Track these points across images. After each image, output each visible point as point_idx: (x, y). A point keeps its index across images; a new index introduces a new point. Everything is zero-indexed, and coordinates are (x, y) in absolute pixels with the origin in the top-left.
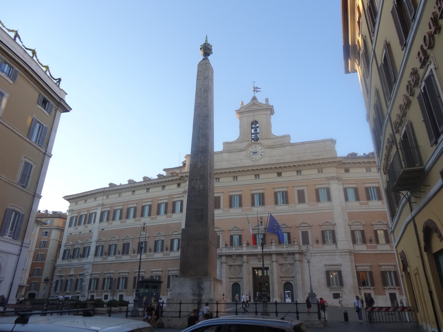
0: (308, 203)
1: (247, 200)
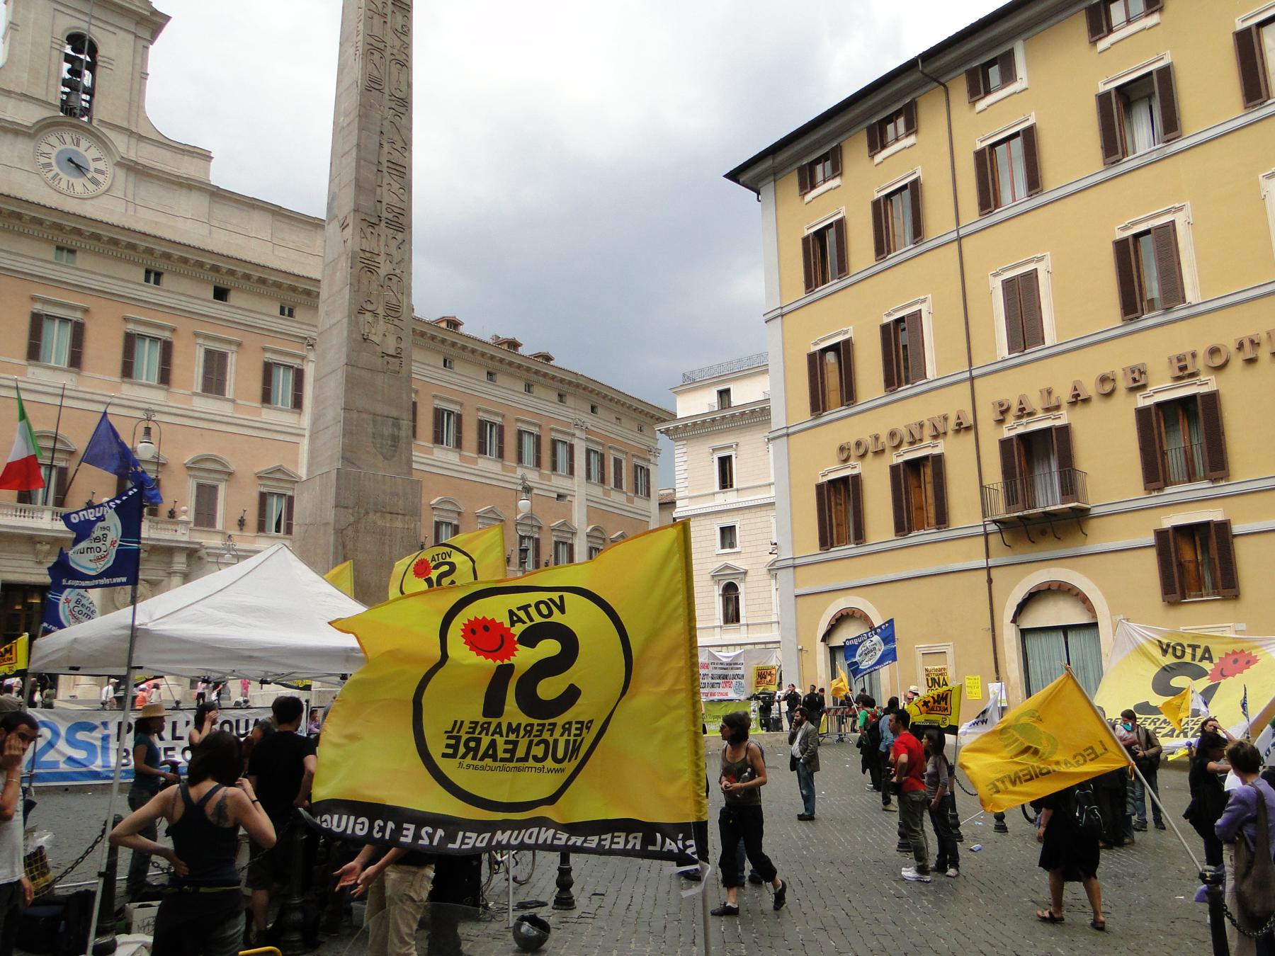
0: (233, 401)
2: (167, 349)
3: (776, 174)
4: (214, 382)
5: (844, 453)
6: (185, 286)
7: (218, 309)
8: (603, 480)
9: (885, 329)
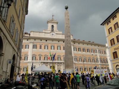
1: (49, 47)
2: (48, 46)
3: (105, 24)
4: (41, 48)
5: (115, 49)
6: (85, 45)
7: (46, 42)
8: (101, 53)
9: (117, 37)
